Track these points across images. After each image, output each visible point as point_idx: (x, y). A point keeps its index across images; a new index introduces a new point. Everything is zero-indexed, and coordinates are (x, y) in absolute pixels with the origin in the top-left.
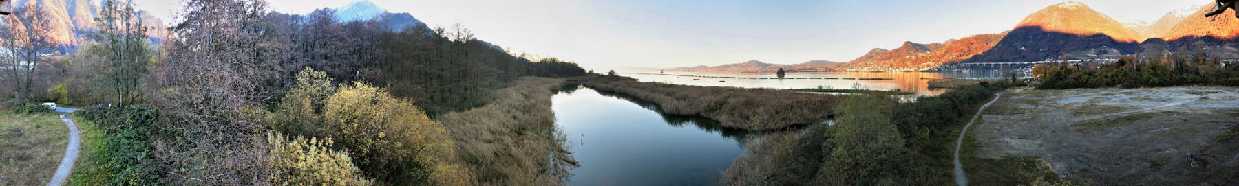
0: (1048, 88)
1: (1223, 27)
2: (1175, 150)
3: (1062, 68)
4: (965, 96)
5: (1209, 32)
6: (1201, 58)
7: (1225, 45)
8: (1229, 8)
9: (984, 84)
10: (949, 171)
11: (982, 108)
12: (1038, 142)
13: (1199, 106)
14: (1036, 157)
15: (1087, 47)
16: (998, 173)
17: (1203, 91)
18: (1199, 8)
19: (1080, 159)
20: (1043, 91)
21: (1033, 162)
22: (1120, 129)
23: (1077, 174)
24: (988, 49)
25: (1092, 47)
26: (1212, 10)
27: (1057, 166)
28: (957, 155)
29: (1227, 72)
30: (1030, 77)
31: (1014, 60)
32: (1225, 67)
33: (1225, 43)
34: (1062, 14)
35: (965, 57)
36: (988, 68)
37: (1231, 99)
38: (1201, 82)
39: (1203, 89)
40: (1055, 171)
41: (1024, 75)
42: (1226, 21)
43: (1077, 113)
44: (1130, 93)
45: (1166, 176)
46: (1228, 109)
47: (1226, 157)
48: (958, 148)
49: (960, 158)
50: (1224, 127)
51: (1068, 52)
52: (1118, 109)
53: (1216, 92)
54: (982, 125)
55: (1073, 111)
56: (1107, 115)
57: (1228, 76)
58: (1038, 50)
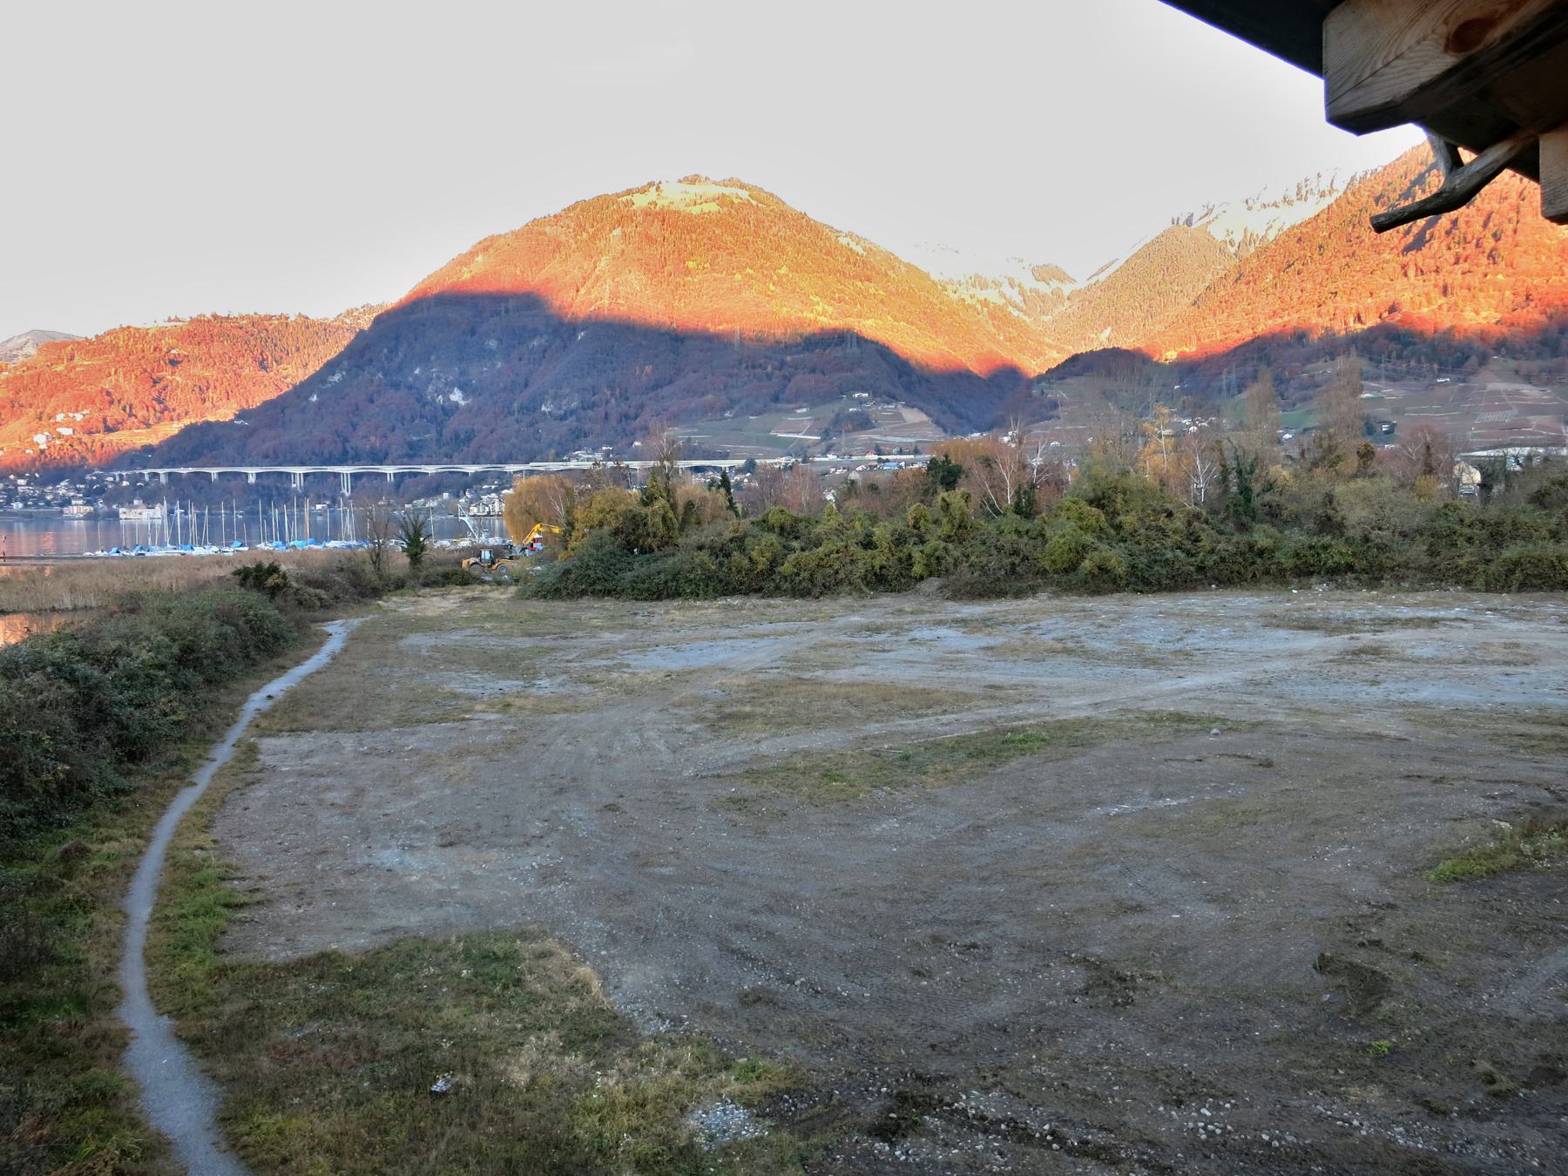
0: (583, 593)
1: (1472, 281)
2: (1211, 912)
3: (648, 500)
4: (157, 648)
5: (1392, 309)
6: (1350, 444)
7: (1485, 374)
8: (1507, 173)
9: (258, 577)
10: (100, 1072)
11: (257, 701)
12: (534, 859)
13: (1339, 691)
14: (524, 936)
15: (776, 399)
16: (366, 1017)
17: (1358, 614)
18: (1341, 187)
19: (740, 941)
20: (560, 606)
21: (509, 958)
22: (932, 801)
23: (722, 1014)
24: (272, 395)
25: (798, 398)
26: (1407, 194)
27: (628, 979)
28: (133, 976)
29: (1493, 513)
30: (495, 541)
31: (413, 453)
32: (1485, 486)
33: (1484, 360)
34: (650, 240)
35: (136, 438)
36: (273, 492)
37: (1518, 657)
38: (1350, 568)
39: (1360, 604)
40: (615, 1002)
41: (460, 530)
42: (1489, 243)
43: (724, 719)
44: (986, 623)
45: (1163, 1040)
46: (1500, 713)
47: (1490, 962)
48: (136, 937)
49: (151, 987)
50: (1478, 804)
51: (675, 419)
52: (923, 700)
53: (1433, 622)
54: (260, 793)
55: (707, 709)
56: (873, 728)
57: (1496, 536)
58: (531, 408)
